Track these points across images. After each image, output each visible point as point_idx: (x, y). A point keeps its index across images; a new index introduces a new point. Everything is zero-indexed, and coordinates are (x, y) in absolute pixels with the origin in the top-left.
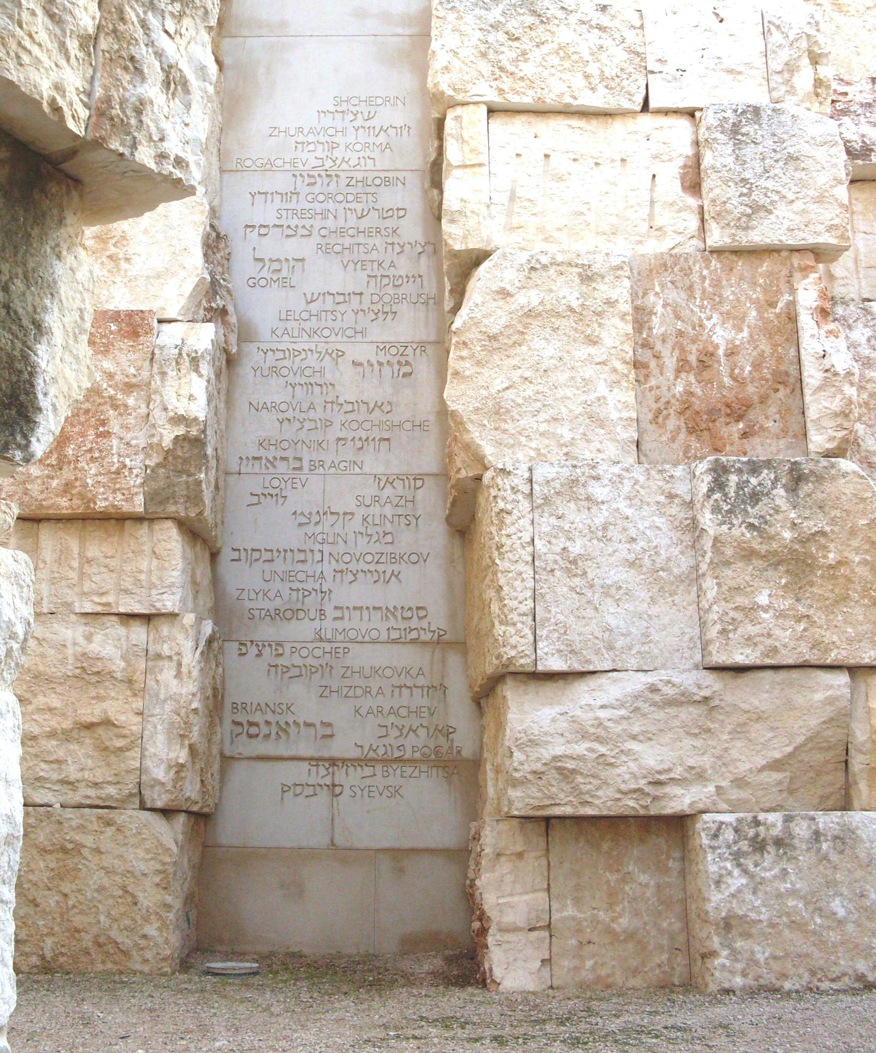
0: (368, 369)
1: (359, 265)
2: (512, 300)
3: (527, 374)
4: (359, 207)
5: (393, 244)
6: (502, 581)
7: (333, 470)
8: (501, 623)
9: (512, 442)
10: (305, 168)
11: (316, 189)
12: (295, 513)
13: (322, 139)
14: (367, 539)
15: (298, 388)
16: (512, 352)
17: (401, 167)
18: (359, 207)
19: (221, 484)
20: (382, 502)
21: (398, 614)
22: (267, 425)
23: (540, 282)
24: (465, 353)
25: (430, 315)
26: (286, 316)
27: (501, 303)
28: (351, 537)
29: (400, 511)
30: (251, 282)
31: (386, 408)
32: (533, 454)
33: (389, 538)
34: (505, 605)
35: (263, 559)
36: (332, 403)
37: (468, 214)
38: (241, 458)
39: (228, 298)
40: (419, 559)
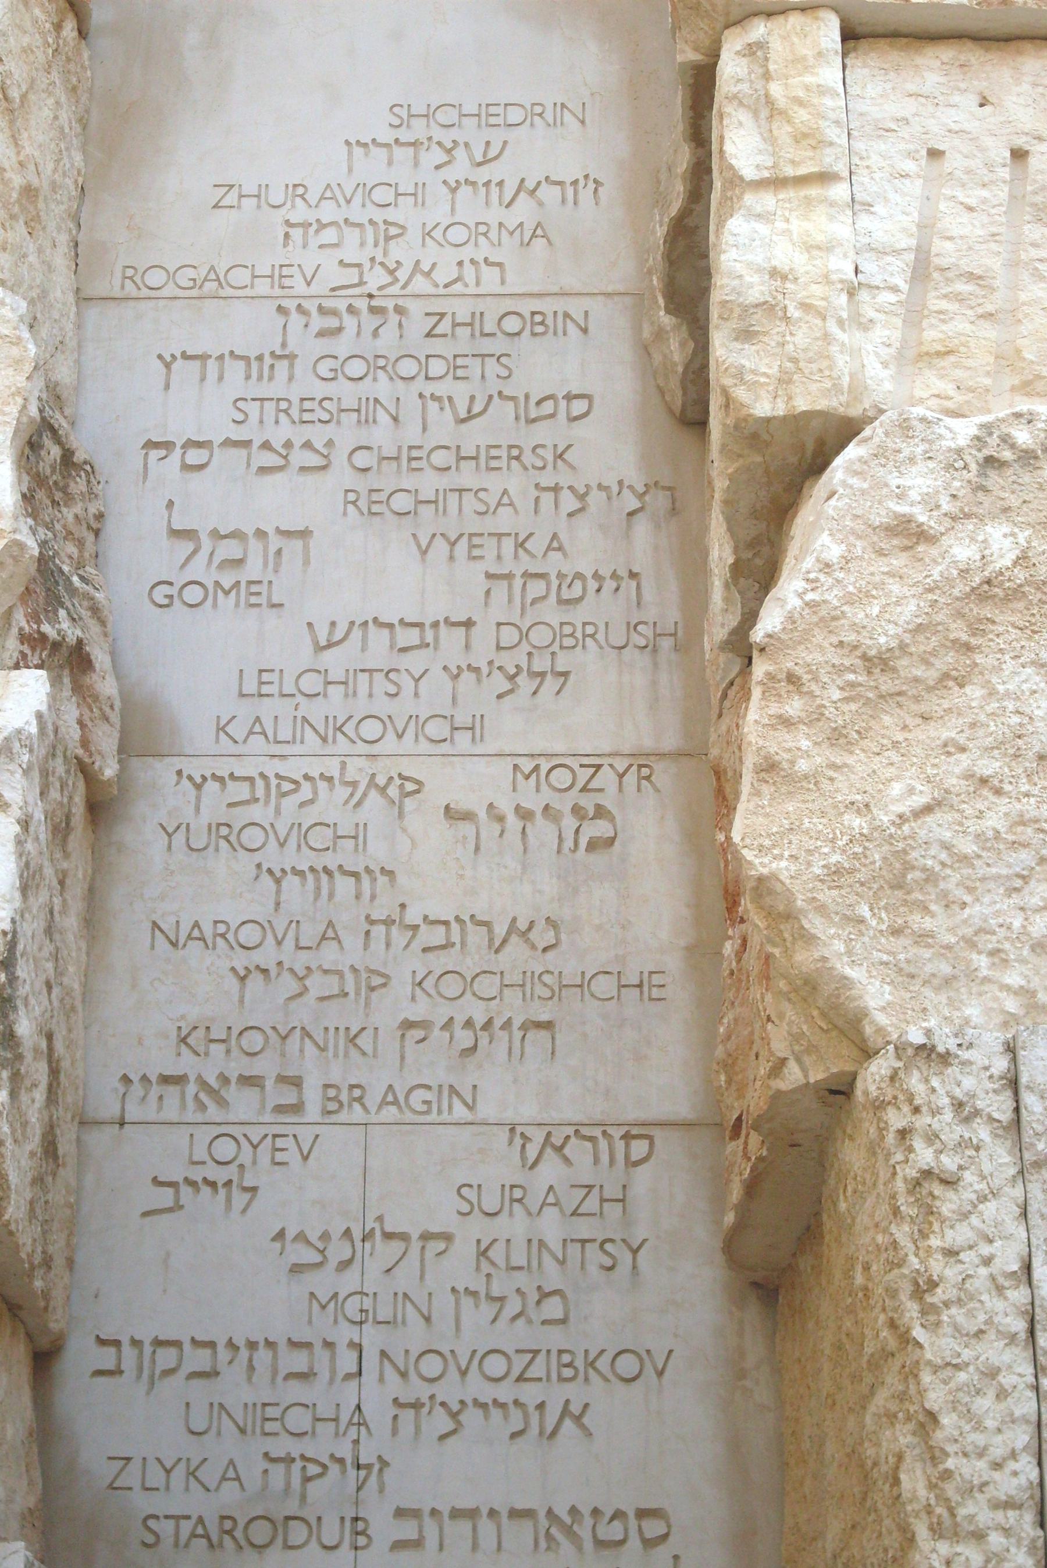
0: (489, 830)
1: (462, 546)
2: (934, 551)
3: (988, 767)
4: (461, 392)
5: (556, 489)
6: (936, 1397)
7: (390, 1113)
8: (937, 1531)
9: (945, 969)
10: (314, 289)
11: (342, 346)
12: (281, 1235)
13: (357, 213)
14: (488, 1310)
15: (291, 882)
16: (934, 704)
17: (578, 287)
18: (461, 392)
19: (65, 1147)
20: (534, 1202)
21: (584, 1532)
22: (204, 987)
23: (1014, 501)
24: (794, 707)
25: (664, 677)
26: (259, 685)
27: (898, 561)
28: (443, 1305)
29: (584, 1229)
30: (159, 595)
31: (542, 936)
32: (1012, 1005)
33: (553, 1308)
34: (947, 1475)
35: (187, 1368)
36: (388, 922)
37: (794, 312)
38: (126, 1079)
39: (95, 628)
40: (644, 1368)
